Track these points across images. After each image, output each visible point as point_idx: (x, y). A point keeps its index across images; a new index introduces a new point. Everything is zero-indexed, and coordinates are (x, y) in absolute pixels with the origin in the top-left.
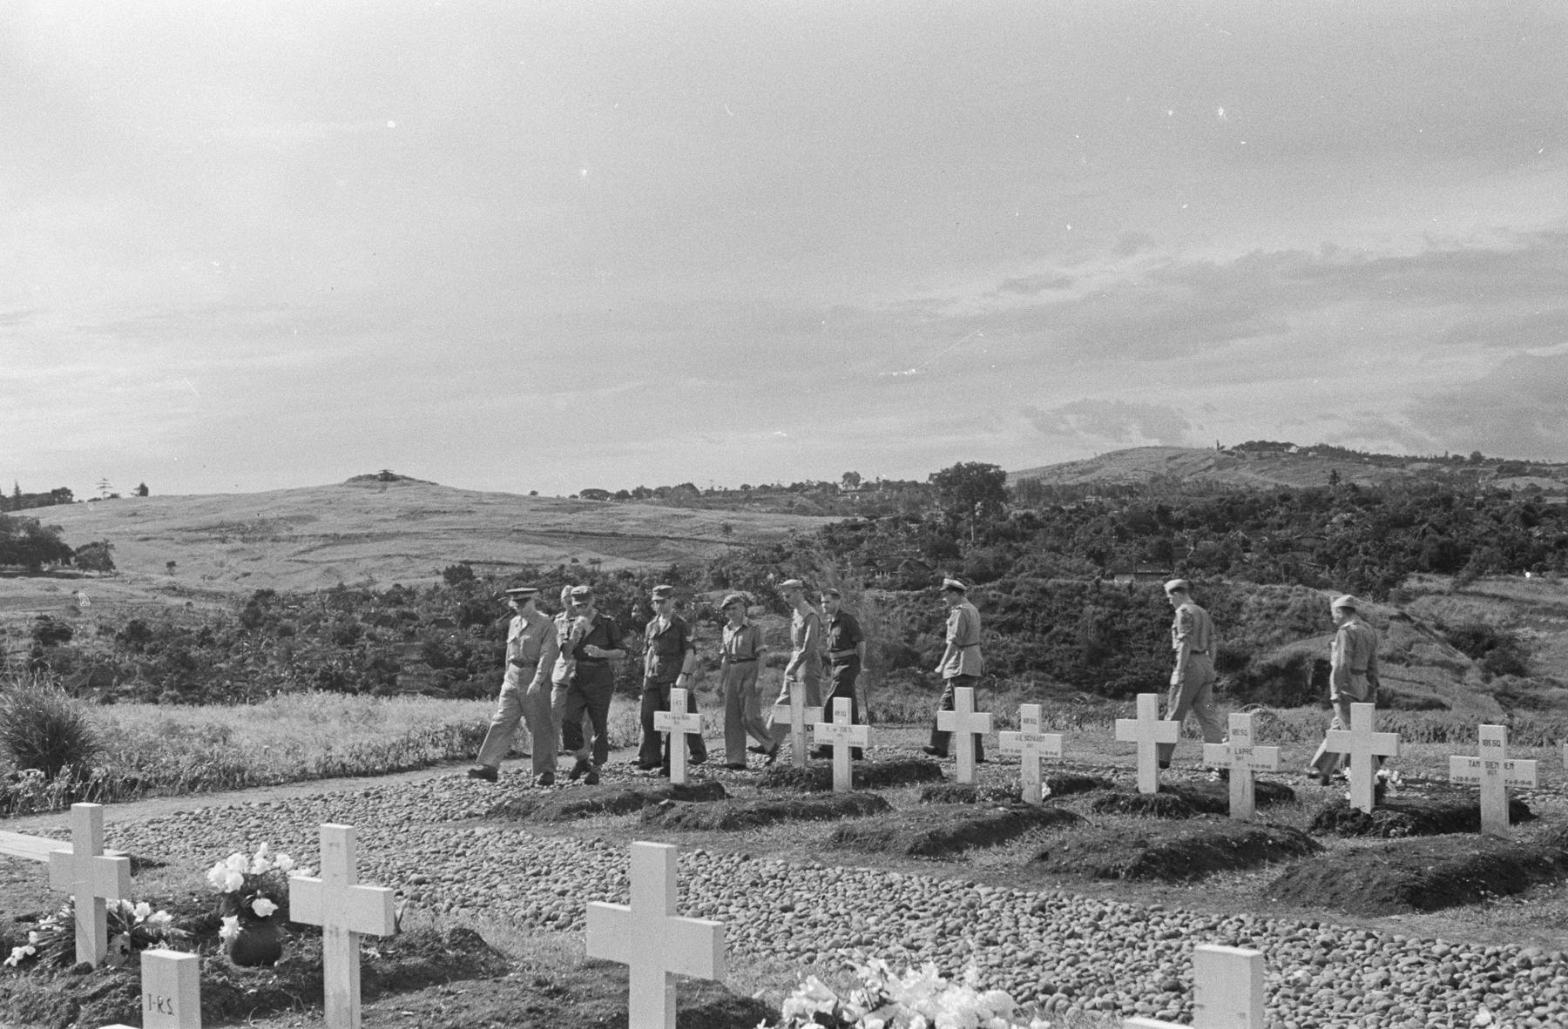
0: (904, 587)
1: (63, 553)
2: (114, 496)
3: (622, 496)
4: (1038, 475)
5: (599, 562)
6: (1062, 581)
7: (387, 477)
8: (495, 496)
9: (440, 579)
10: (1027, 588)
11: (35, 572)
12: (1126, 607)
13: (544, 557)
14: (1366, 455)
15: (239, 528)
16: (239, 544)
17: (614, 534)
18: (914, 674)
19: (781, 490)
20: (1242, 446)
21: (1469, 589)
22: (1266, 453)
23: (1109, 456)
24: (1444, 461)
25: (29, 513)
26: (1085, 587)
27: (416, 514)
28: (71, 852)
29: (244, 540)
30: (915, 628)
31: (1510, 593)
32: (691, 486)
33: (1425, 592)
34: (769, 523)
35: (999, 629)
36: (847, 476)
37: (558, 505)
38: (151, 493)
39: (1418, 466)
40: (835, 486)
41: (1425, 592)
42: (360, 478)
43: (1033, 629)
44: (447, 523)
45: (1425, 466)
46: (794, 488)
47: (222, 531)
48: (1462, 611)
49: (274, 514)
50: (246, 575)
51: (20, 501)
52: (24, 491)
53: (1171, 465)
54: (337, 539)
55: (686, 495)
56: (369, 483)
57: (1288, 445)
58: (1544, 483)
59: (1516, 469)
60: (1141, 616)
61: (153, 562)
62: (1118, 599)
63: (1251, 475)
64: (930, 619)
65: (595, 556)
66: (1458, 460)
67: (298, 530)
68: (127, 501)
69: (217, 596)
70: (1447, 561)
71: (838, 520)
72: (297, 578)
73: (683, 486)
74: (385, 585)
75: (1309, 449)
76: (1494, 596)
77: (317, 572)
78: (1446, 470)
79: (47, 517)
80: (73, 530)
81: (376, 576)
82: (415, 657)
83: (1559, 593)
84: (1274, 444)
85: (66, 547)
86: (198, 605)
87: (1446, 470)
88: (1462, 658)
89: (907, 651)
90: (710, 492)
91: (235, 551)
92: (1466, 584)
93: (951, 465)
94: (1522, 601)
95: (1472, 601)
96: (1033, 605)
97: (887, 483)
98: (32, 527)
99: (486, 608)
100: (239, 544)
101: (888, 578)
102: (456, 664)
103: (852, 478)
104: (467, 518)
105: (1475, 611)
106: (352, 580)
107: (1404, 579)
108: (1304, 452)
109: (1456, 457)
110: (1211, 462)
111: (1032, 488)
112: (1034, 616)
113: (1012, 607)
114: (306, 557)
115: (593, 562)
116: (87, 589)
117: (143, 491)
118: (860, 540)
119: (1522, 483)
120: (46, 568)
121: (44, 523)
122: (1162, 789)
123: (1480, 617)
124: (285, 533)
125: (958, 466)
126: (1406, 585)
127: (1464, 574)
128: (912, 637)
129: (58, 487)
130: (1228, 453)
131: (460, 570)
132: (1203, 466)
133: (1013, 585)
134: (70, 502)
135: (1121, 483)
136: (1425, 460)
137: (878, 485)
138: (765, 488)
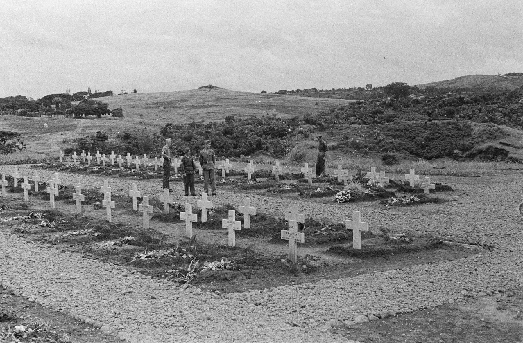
1: (108, 112)
2: (126, 93)
3: (292, 92)
6: (415, 122)
7: (211, 87)
9: (224, 120)
11: (99, 117)
15: (163, 104)
19: (345, 90)
22: (515, 77)
25: (99, 99)
27: (219, 99)
29: (165, 108)
34: (334, 101)
37: (271, 96)
38: (137, 92)
40: (363, 89)
42: (201, 88)
47: (157, 105)
51: (97, 95)
52: (98, 92)
53: (482, 81)
54: (194, 107)
55: (315, 92)
61: (136, 114)
65: (275, 113)
68: (130, 95)
69: (155, 126)
71: (354, 101)
74: (207, 122)
77: (186, 118)
79: (103, 100)
80: (111, 103)
84: (518, 74)
85: (109, 110)
86: (149, 128)
91: (162, 111)
93: (390, 83)
97: (381, 88)
98: (99, 103)
103: (369, 86)
106: (197, 120)
110: (495, 80)
115: (274, 115)
116: (116, 122)
117: (135, 91)
118: (360, 108)
120: (102, 116)
121: (103, 102)
122: (415, 185)
125: (393, 83)
129: (109, 90)
130: (502, 77)
132: (493, 81)
134: (112, 95)
135: (462, 87)
137: (378, 88)
138: (340, 89)
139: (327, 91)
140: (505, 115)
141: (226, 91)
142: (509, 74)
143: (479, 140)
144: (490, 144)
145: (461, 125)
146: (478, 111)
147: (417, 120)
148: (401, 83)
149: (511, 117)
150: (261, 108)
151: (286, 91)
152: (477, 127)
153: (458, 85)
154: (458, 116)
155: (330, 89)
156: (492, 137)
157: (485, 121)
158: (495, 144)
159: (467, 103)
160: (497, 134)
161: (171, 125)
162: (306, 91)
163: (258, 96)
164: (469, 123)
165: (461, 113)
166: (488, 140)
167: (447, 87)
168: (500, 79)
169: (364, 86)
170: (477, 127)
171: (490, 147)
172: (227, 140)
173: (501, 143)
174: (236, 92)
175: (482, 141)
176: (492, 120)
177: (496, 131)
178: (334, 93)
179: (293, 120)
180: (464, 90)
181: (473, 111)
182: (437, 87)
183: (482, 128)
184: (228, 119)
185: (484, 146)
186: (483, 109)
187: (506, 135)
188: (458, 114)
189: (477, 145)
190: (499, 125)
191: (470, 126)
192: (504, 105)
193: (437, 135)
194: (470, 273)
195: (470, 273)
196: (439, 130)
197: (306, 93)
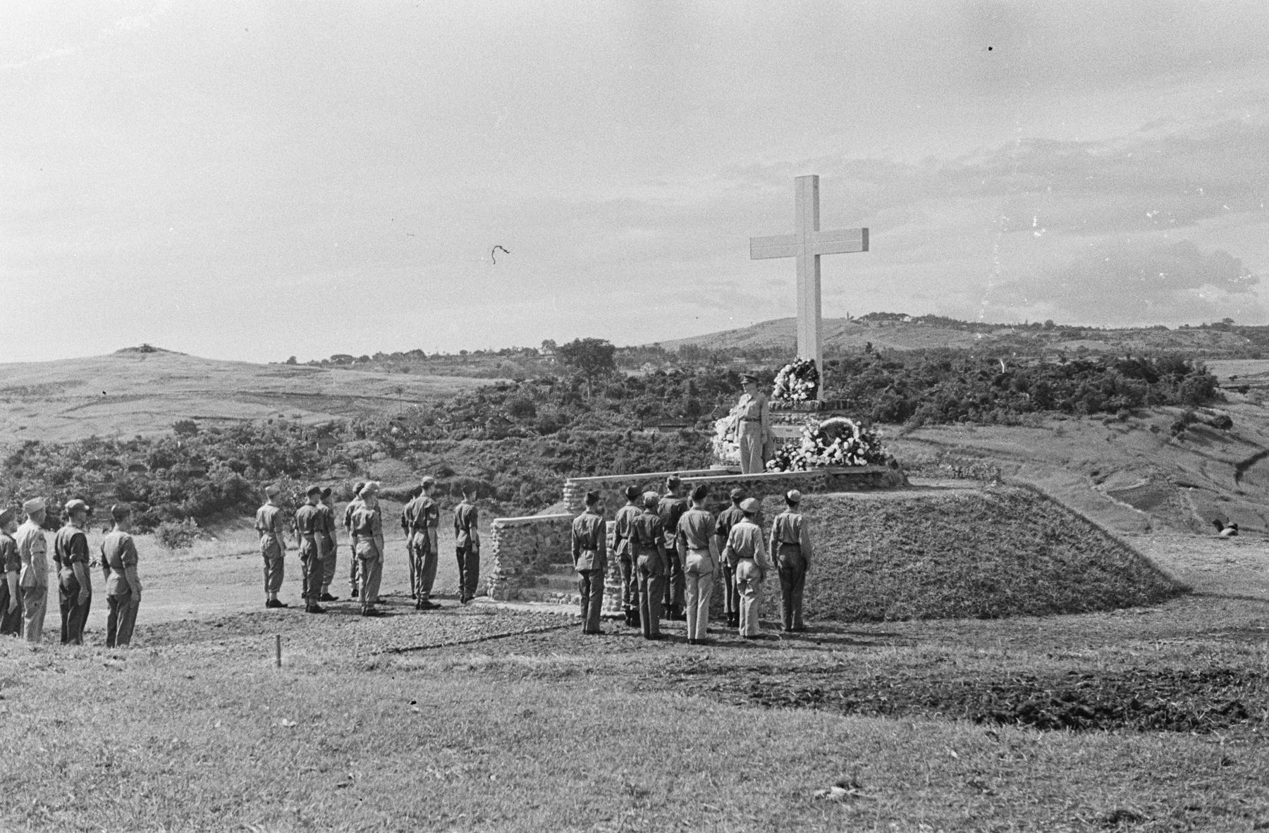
0: (491, 438)
5: (299, 417)
6: (604, 432)
7: (147, 349)
8: (231, 364)
9: (172, 431)
10: (578, 438)
12: (650, 451)
13: (258, 413)
14: (965, 323)
15: (21, 391)
16: (19, 404)
17: (318, 395)
18: (489, 503)
19: (492, 354)
20: (867, 317)
22: (885, 323)
23: (762, 326)
24: (1025, 327)
26: (621, 437)
28: (663, 622)
29: (24, 401)
30: (494, 468)
31: (937, 439)
32: (420, 352)
34: (446, 383)
35: (555, 469)
36: (545, 343)
39: (1004, 332)
40: (536, 351)
42: (125, 350)
43: (580, 468)
44: (188, 386)
45: (1010, 332)
46: (503, 353)
49: (51, 380)
50: (22, 428)
56: (132, 353)
57: (904, 315)
58: (1090, 345)
59: (1074, 334)
60: (659, 458)
62: (645, 446)
64: (506, 462)
65: (297, 412)
66: (1036, 326)
67: (70, 392)
71: (492, 382)
72: (63, 430)
73: (414, 352)
75: (918, 319)
76: (927, 441)
78: (1024, 334)
81: (124, 429)
82: (110, 494)
83: (975, 438)
84: (892, 315)
87: (1024, 334)
89: (486, 486)
90: (436, 357)
92: (909, 431)
93: (571, 340)
94: (945, 445)
95: (912, 445)
96: (581, 451)
99: (170, 455)
100: (19, 404)
101: (480, 430)
102: (140, 500)
104: (203, 382)
105: (911, 452)
108: (916, 320)
109: (1035, 325)
110: (842, 329)
111: (636, 355)
112: (581, 458)
113: (567, 452)
114: (71, 414)
118: (503, 398)
119: (1074, 345)
123: (914, 457)
124: (59, 395)
125: (577, 341)
127: (907, 424)
128: (491, 475)
130: (856, 322)
131: (186, 424)
132: (837, 332)
133: (568, 436)
136: (1010, 327)
138: (478, 353)
139: (448, 357)
141: (183, 359)
147: (932, 394)
148: (595, 341)
150: (265, 400)
151: (350, 359)
153: (761, 340)
155: (455, 351)
161: (36, 443)
162: (396, 357)
163: (262, 372)
169: (536, 344)
172: (160, 482)
174: (208, 363)
178: (464, 362)
179: (330, 428)
184: (186, 428)
197: (399, 362)
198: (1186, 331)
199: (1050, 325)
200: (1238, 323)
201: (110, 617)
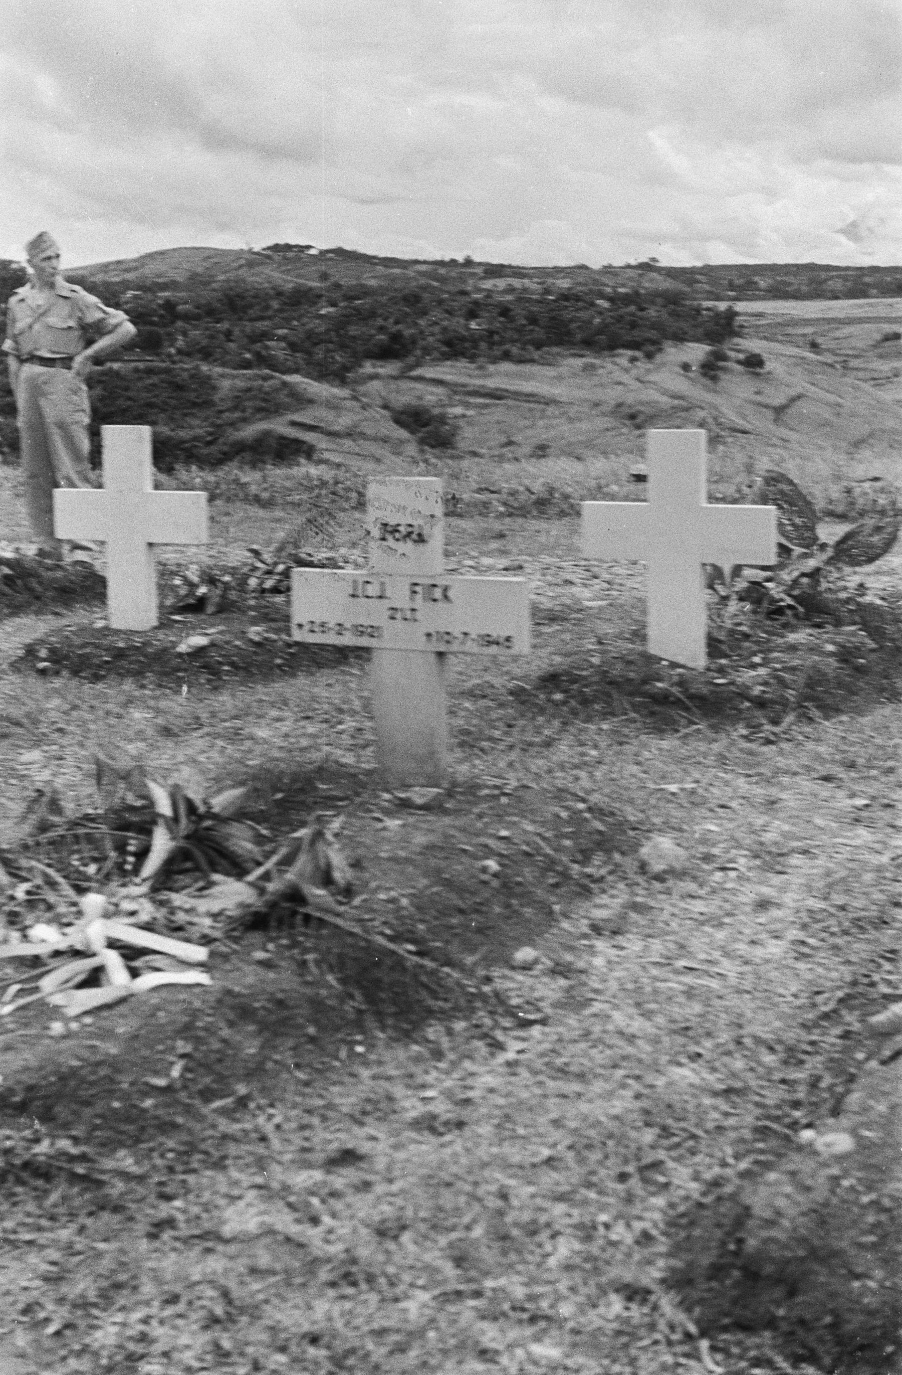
4: (84, 272)
14: (375, 257)
20: (269, 248)
21: (414, 373)
22: (290, 254)
23: (151, 256)
24: (441, 263)
33: (375, 377)
39: (423, 268)
41: (375, 377)
48: (407, 394)
57: (309, 247)
63: (276, 275)
70: (393, 349)
78: (442, 271)
87: (442, 271)
88: (403, 434)
105: (418, 393)
107: (361, 366)
110: (243, 262)
123: (420, 398)
126: (361, 371)
127: (411, 360)
132: (235, 265)
135: (160, 280)
140: (293, 347)
142: (276, 248)
143: (237, 414)
144: (263, 426)
145: (185, 375)
146: (222, 337)
149: (309, 353)
152: (228, 381)
153: (148, 270)
154: (173, 351)
156: (269, 406)
157: (247, 365)
158: (280, 426)
159: (187, 317)
160: (283, 397)
164: (205, 368)
165: (180, 342)
166: (258, 416)
167: (117, 279)
168: (255, 260)
170: (228, 381)
171: (267, 434)
173: (294, 424)
175: (245, 420)
176: (262, 360)
177: (277, 390)
180: (164, 287)
181: (212, 337)
182: (92, 279)
183: (240, 384)
185: (249, 431)
186: (236, 332)
187: (302, 401)
188: (172, 346)
189: (230, 430)
190: (283, 373)
191: (209, 377)
192: (288, 320)
193: (122, 403)
194: (753, 942)
195: (753, 942)
196: (127, 389)
198: (608, 270)
199: (469, 262)
200: (664, 263)
201: (245, 1233)
